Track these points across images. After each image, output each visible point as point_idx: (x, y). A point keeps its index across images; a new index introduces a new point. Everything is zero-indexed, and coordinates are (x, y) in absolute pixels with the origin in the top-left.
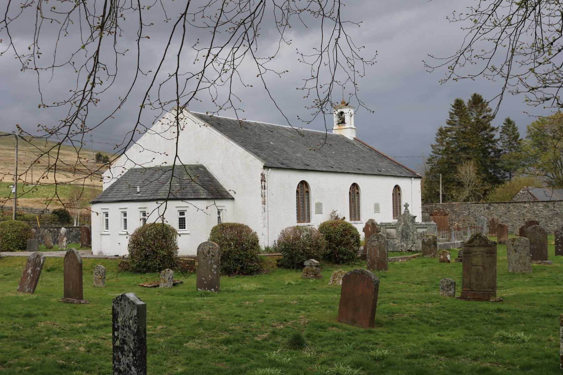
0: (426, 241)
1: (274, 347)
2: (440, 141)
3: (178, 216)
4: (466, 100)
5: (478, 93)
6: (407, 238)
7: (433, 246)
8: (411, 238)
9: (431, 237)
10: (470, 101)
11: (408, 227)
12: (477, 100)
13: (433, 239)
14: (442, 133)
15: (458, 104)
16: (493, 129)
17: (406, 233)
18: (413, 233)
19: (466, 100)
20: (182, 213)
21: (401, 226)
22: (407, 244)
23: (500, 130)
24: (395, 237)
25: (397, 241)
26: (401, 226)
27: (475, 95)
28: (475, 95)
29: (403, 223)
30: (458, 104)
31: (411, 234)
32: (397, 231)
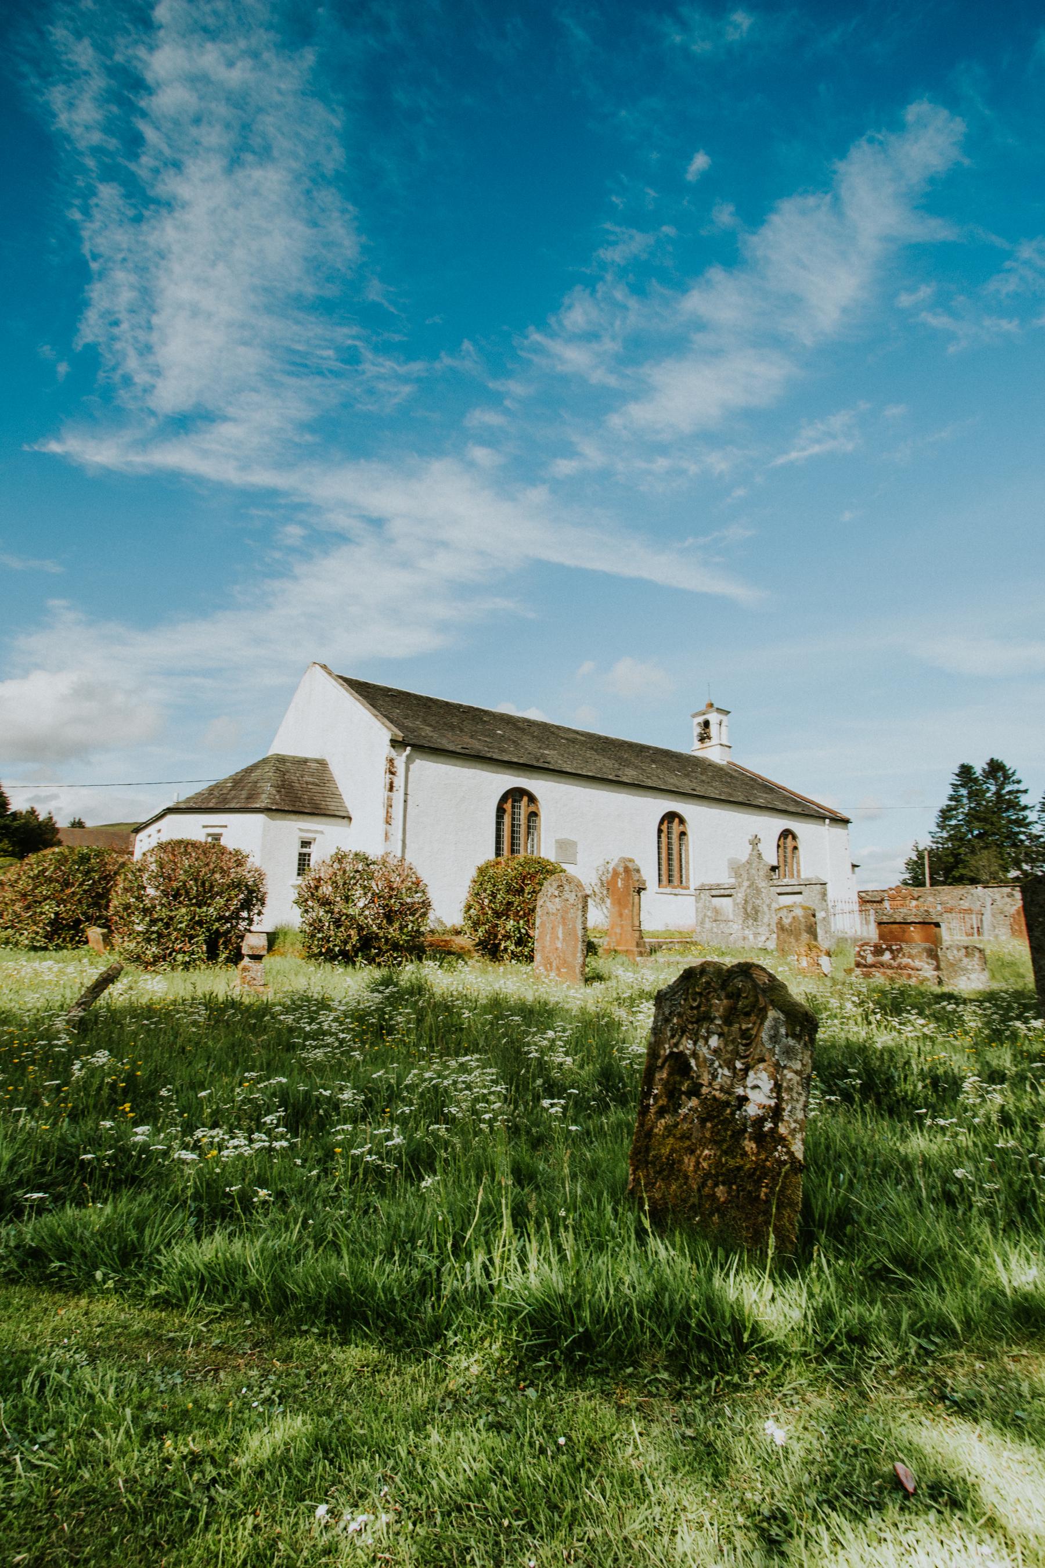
0: (786, 921)
1: (489, 1190)
2: (942, 827)
3: (296, 849)
4: (979, 768)
5: (997, 757)
6: (756, 920)
7: (805, 937)
8: (766, 920)
9: (799, 912)
10: (984, 770)
11: (758, 891)
12: (995, 768)
13: (806, 917)
14: (946, 814)
15: (965, 771)
16: (1025, 808)
17: (754, 908)
18: (769, 906)
19: (979, 768)
20: (305, 844)
21: (743, 889)
22: (756, 935)
23: (1038, 808)
24: (731, 917)
25: (735, 926)
26: (743, 889)
27: (992, 760)
28: (992, 760)
29: (746, 884)
30: (965, 771)
31: (766, 909)
32: (736, 904)
